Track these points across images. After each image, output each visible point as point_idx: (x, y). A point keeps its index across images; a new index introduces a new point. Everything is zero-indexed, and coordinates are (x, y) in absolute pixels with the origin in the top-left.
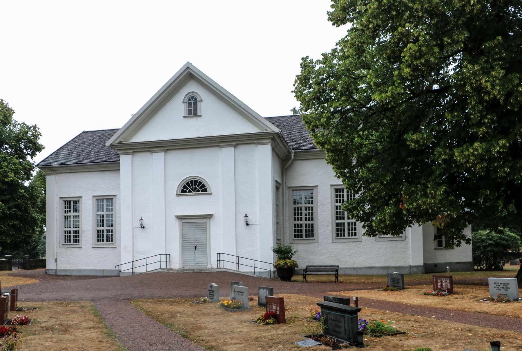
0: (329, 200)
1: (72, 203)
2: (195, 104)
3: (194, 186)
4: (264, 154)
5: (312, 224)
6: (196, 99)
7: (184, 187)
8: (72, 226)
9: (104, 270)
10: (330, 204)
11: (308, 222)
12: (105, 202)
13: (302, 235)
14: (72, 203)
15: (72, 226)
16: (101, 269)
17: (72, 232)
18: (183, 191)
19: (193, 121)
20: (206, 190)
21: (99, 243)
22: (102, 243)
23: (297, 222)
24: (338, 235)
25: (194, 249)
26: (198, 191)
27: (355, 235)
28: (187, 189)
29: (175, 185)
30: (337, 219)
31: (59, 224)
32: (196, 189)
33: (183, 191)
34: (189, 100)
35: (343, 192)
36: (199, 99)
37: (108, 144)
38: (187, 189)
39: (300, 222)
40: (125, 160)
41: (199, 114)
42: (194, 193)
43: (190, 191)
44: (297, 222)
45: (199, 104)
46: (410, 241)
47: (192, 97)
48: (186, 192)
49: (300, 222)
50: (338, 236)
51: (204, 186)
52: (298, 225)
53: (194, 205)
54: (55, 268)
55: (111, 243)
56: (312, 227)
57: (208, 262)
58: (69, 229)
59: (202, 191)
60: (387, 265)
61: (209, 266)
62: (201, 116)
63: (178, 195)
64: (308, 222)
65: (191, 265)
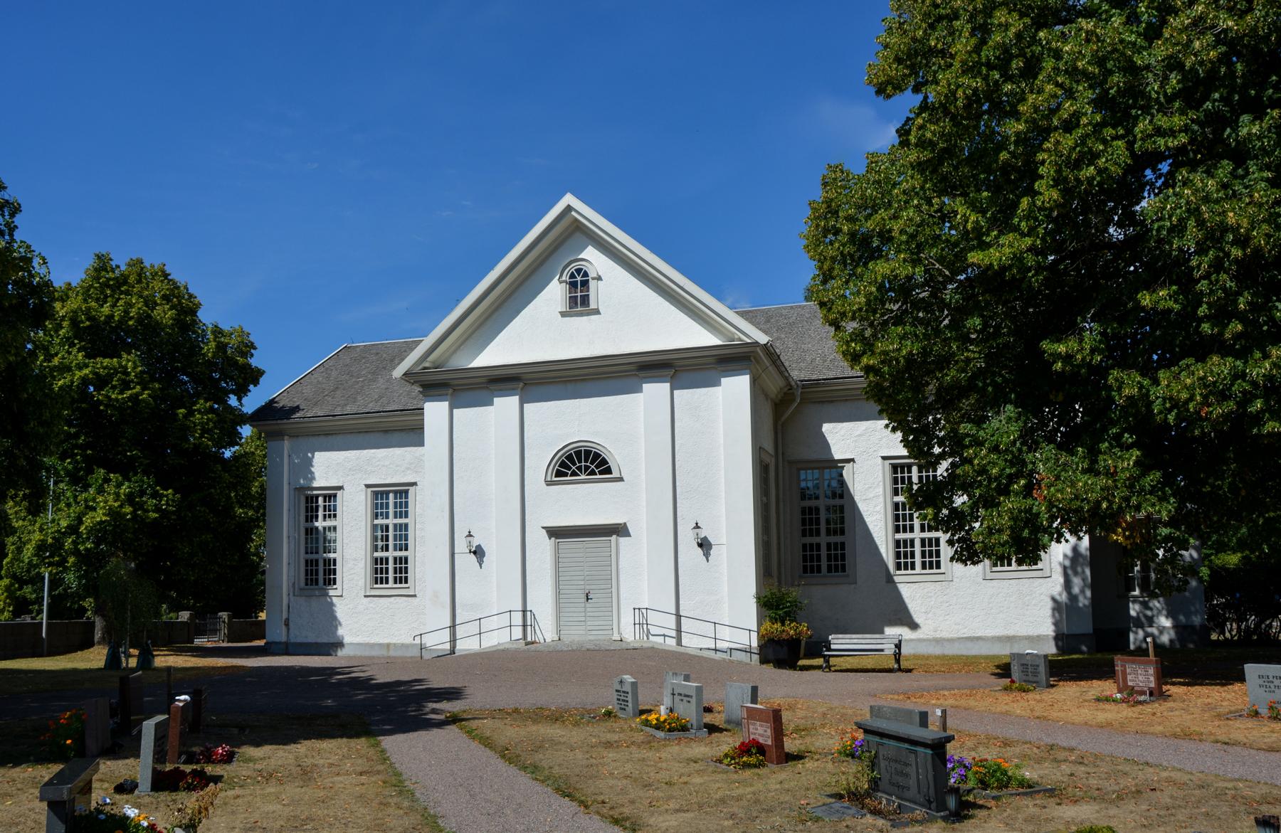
2: (585, 284)
3: (582, 463)
4: (735, 392)
5: (843, 544)
6: (586, 274)
7: (563, 464)
9: (388, 645)
10: (881, 499)
12: (391, 499)
18: (559, 474)
20: (608, 471)
21: (398, 585)
26: (593, 473)
28: (569, 468)
29: (541, 460)
30: (897, 530)
32: (587, 468)
34: (572, 276)
36: (592, 274)
37: (398, 372)
38: (569, 468)
40: (435, 412)
41: (593, 305)
42: (583, 477)
43: (574, 474)
45: (592, 284)
47: (579, 271)
48: (566, 475)
51: (604, 462)
53: (584, 503)
54: (284, 639)
55: (403, 585)
59: (601, 473)
60: (1011, 633)
62: (597, 312)
63: (549, 483)
65: (577, 635)
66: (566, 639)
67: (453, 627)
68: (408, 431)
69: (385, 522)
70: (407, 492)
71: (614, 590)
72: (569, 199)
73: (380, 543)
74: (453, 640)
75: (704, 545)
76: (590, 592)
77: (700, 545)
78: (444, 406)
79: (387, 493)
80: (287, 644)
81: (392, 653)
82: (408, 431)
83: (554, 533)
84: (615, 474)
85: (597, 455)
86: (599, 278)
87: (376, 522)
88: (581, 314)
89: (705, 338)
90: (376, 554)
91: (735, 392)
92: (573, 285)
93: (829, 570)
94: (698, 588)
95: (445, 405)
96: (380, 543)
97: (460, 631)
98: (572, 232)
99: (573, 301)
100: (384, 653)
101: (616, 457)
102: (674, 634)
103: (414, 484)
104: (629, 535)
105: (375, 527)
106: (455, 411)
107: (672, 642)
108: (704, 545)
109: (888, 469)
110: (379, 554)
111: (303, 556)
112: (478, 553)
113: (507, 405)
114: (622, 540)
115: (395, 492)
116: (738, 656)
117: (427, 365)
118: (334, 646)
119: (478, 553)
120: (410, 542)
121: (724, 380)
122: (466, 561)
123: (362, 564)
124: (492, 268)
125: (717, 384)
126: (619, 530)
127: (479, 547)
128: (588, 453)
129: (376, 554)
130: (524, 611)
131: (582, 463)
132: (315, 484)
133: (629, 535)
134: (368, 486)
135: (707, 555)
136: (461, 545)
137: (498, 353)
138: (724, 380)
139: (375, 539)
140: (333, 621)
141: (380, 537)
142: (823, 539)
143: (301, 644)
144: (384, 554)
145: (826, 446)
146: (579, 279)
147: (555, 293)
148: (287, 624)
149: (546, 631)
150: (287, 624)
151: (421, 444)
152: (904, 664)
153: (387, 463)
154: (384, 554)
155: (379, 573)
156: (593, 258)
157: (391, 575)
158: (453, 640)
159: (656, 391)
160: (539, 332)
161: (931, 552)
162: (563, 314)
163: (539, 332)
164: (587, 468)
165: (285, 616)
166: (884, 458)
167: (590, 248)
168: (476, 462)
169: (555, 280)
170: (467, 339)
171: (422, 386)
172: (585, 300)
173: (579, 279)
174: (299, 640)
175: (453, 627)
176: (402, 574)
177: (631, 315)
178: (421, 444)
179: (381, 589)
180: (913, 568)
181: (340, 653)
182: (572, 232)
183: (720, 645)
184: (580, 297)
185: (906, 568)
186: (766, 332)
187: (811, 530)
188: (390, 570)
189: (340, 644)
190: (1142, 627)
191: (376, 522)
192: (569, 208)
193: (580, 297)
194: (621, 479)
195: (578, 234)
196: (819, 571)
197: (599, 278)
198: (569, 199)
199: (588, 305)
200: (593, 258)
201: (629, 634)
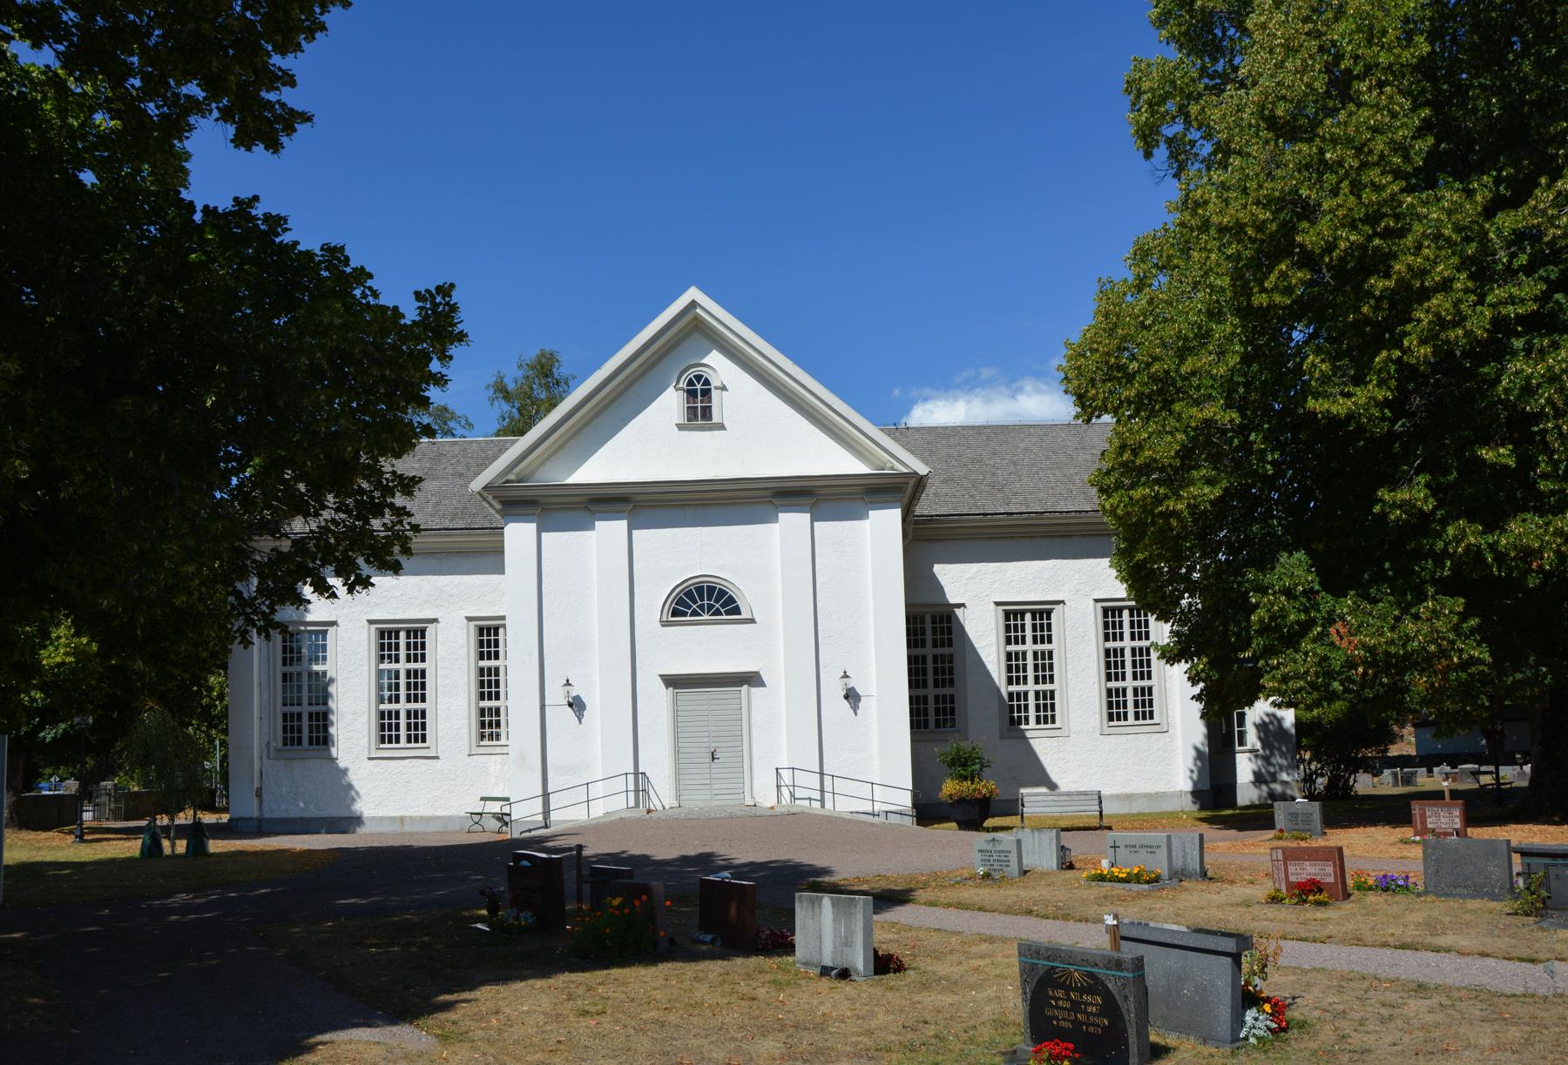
0: (993, 638)
1: (402, 635)
2: (706, 393)
3: (704, 601)
4: (886, 523)
5: (952, 697)
6: (707, 382)
7: (680, 602)
8: (305, 701)
9: (402, 819)
10: (994, 648)
11: (941, 691)
13: (398, 737)
14: (402, 635)
15: (305, 701)
16: (393, 814)
17: (305, 718)
18: (675, 613)
19: (701, 439)
20: (737, 611)
21: (413, 745)
22: (1122, 723)
23: (419, 706)
24: (1111, 718)
25: (709, 759)
26: (718, 613)
27: (424, 741)
28: (689, 607)
29: (654, 599)
30: (482, 697)
31: (265, 695)
32: (710, 607)
33: (675, 613)
34: (690, 383)
35: (397, 637)
36: (714, 383)
37: (477, 484)
38: (689, 607)
39: (413, 706)
40: (519, 536)
41: (716, 419)
42: (706, 617)
43: (695, 613)
44: (419, 706)
45: (715, 394)
46: (1179, 734)
47: (699, 378)
48: (685, 614)
49: (413, 706)
50: (383, 742)
51: (731, 600)
52: (416, 712)
53: (707, 647)
54: (255, 814)
55: (420, 745)
56: (952, 702)
57: (747, 790)
58: (296, 709)
59: (727, 613)
60: (1128, 790)
61: (749, 801)
62: (721, 427)
63: (665, 624)
64: (941, 691)
65: (701, 800)
66: (686, 805)
67: (546, 795)
68: (489, 557)
69: (394, 666)
70: (423, 631)
71: (746, 747)
72: (693, 294)
73: (387, 693)
74: (546, 812)
75: (852, 696)
76: (717, 752)
77: (846, 697)
78: (531, 528)
79: (1023, 613)
80: (260, 820)
81: (407, 828)
82: (489, 557)
83: (672, 681)
84: (744, 615)
85: (722, 593)
86: (724, 388)
87: (382, 666)
88: (702, 428)
89: (853, 466)
90: (382, 707)
91: (886, 523)
92: (691, 394)
93: (938, 726)
94: (828, 747)
95: (622, 525)
96: (387, 693)
97: (554, 801)
98: (694, 331)
99: (692, 413)
100: (397, 828)
101: (747, 598)
102: (817, 795)
103: (435, 621)
104: (763, 685)
105: (380, 673)
106: (635, 532)
107: (816, 805)
108: (852, 696)
109: (1001, 615)
110: (386, 707)
111: (280, 708)
112: (577, 705)
113: (612, 531)
114: (754, 690)
115: (1034, 613)
116: (894, 819)
117: (511, 477)
118: (351, 822)
119: (577, 705)
120: (429, 692)
121: (597, 523)
122: (560, 715)
123: (364, 718)
124: (599, 367)
125: (590, 527)
126: (752, 679)
127: (577, 698)
128: (711, 589)
129: (382, 707)
130: (636, 773)
131: (704, 601)
132: (310, 618)
133: (763, 685)
134: (371, 622)
135: (855, 709)
136: (556, 696)
137: (602, 467)
138: (597, 523)
139: (380, 688)
140: (346, 791)
141: (387, 688)
142: (403, 706)
143: (282, 820)
144: (393, 707)
145: (940, 589)
146: (699, 387)
147: (671, 402)
148: (259, 794)
149: (663, 795)
150: (259, 794)
151: (500, 569)
152: (1105, 822)
153: (397, 594)
154: (393, 707)
155: (387, 729)
156: (718, 365)
157: (403, 732)
158: (546, 812)
159: (793, 523)
160: (649, 446)
161: (1045, 705)
162: (680, 427)
163: (649, 446)
164: (710, 607)
165: (256, 784)
166: (998, 604)
167: (714, 352)
168: (575, 594)
169: (671, 389)
170: (553, 454)
171: (502, 503)
172: (707, 413)
173: (699, 387)
174: (277, 815)
175: (546, 795)
176: (418, 729)
177: (763, 433)
178: (500, 569)
179: (389, 750)
180: (398, 741)
181: (361, 830)
182: (694, 331)
183: (878, 807)
184: (700, 407)
185: (390, 742)
186: (923, 460)
187: (490, 693)
188: (401, 725)
189: (357, 820)
190: (1266, 783)
191: (382, 666)
192: (693, 304)
193: (700, 407)
194: (752, 621)
195: (697, 335)
196: (300, 743)
197: (724, 388)
198: (693, 294)
199: (710, 418)
200: (718, 365)
201: (765, 796)
